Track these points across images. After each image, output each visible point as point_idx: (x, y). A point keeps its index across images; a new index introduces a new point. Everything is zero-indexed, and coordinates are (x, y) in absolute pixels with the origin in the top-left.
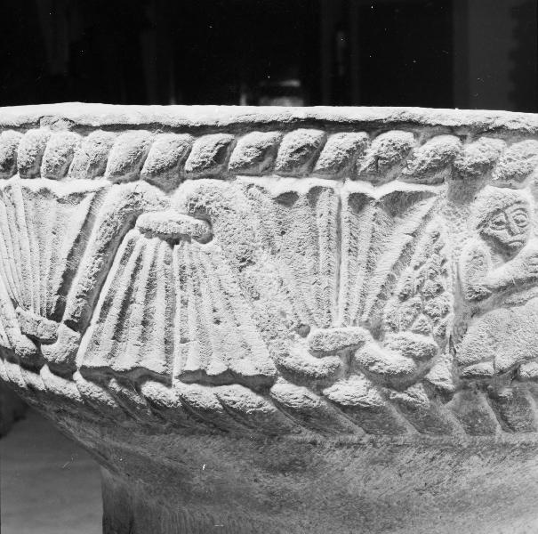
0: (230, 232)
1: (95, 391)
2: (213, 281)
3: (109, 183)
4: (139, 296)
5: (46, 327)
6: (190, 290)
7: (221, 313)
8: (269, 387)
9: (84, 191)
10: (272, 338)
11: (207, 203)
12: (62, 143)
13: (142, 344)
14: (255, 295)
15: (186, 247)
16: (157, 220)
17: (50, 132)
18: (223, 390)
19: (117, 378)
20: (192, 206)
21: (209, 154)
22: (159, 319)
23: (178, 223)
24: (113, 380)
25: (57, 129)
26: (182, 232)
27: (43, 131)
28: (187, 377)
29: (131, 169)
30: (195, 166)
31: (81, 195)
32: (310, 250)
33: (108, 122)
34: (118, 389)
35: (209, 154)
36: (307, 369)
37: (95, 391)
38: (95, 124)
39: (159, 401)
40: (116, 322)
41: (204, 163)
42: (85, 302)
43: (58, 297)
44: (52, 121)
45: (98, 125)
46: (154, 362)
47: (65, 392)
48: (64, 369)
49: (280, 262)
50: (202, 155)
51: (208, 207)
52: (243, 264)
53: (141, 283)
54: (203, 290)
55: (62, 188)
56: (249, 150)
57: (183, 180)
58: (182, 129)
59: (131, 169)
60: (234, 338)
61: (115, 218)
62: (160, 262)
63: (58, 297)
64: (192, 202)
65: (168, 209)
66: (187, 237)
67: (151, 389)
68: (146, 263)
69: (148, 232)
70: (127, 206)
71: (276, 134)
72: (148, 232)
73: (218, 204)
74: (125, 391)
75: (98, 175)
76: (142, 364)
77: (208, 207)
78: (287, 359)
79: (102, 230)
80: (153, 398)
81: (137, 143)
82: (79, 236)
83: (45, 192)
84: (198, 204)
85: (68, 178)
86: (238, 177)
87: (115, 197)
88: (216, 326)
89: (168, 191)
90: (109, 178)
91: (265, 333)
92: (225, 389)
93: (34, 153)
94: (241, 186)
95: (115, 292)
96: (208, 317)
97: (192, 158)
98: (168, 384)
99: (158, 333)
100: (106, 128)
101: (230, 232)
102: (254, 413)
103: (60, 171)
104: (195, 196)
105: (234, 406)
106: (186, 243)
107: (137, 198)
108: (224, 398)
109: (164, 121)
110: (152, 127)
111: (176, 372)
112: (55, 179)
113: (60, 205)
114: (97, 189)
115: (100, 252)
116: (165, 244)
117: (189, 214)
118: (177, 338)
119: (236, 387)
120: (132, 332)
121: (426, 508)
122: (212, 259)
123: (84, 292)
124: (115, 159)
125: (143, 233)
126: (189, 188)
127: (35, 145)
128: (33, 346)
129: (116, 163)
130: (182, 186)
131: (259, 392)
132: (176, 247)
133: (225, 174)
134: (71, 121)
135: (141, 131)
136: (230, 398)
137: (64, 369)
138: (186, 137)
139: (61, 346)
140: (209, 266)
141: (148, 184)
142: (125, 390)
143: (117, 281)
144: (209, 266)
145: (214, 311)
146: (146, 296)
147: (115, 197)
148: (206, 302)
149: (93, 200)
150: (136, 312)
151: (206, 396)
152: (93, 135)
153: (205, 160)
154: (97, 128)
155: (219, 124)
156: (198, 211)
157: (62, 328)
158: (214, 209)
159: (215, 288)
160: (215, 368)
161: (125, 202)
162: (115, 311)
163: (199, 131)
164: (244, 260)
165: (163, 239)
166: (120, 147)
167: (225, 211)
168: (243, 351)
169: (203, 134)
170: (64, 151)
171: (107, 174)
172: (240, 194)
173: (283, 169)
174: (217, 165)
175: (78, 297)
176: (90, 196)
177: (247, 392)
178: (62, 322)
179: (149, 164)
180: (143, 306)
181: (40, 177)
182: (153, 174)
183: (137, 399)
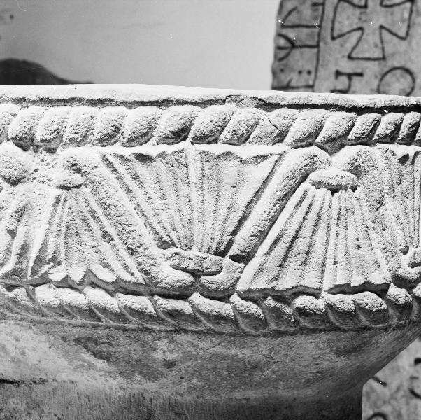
0: (374, 183)
1: (251, 308)
2: (358, 218)
3: (289, 148)
4: (306, 232)
5: (210, 262)
6: (342, 226)
7: (363, 242)
8: (386, 291)
9: (268, 153)
10: (393, 256)
11: (363, 163)
12: (251, 117)
13: (303, 269)
14: (384, 227)
15: (342, 193)
16: (328, 175)
17: (236, 108)
18: (359, 297)
19: (273, 296)
20: (353, 164)
21: (368, 127)
22: (318, 247)
23: (342, 177)
24: (269, 298)
25: (243, 106)
26: (344, 183)
27: (229, 107)
28: (333, 291)
29: (308, 140)
30: (357, 136)
31: (265, 157)
32: (411, 196)
33: (294, 102)
34: (272, 305)
35: (368, 127)
36: (409, 276)
37: (251, 308)
38: (283, 103)
39: (312, 310)
40: (284, 253)
41: (364, 133)
42: (257, 239)
43: (230, 237)
44: (239, 99)
45: (286, 103)
46: (310, 281)
47: (222, 312)
48: (223, 295)
49: (396, 203)
50: (364, 127)
51: (363, 165)
52: (379, 205)
53: (309, 223)
54: (350, 226)
55: (246, 151)
56: (389, 126)
57: (343, 146)
58: (349, 109)
59: (308, 140)
60: (369, 259)
61: (296, 173)
62: (326, 206)
63: (230, 237)
64: (353, 162)
65: (335, 167)
66: (345, 188)
67: (302, 301)
68: (315, 209)
69: (318, 184)
70: (307, 165)
71: (400, 115)
72: (318, 184)
73: (369, 163)
74: (279, 305)
75: (278, 142)
76: (302, 283)
77: (363, 165)
78: (399, 270)
79: (284, 183)
80: (306, 308)
81: (318, 118)
82: (260, 188)
83: (228, 154)
84: (357, 164)
85: (247, 143)
86: (378, 144)
87: (295, 159)
88: (358, 251)
89: (331, 154)
90: (290, 145)
91: (388, 253)
92: (360, 295)
93: (221, 124)
94: (381, 151)
95: (286, 230)
96: (352, 243)
97: (229, 128)
98: (317, 296)
99: (315, 258)
100: (291, 106)
101: (374, 183)
102: (378, 310)
103: (241, 138)
104: (356, 157)
105: (367, 307)
106: (344, 191)
107: (316, 159)
108: (359, 302)
109: (340, 103)
110: (42, 101)
111: (327, 285)
112: (235, 145)
113: (241, 165)
114: (281, 152)
115: (279, 200)
116: (329, 192)
117: (348, 171)
118: (330, 262)
119: (367, 293)
120: (295, 262)
121: (285, 389)
122: (357, 201)
123: (260, 231)
124: (295, 132)
125: (313, 185)
126: (349, 152)
127: (222, 118)
128: (192, 279)
129: (301, 133)
130: (343, 150)
131: (380, 296)
132: (336, 195)
133: (369, 142)
134: (259, 100)
135: (320, 110)
136: (364, 302)
137: (223, 295)
138: (353, 114)
139: (227, 275)
140: (357, 207)
141: (19, 149)
142: (280, 304)
143: (288, 220)
144: (357, 207)
145: (357, 240)
146: (313, 232)
147: (295, 159)
148: (352, 233)
149: (277, 161)
150: (301, 245)
151: (346, 302)
152: (276, 112)
153: (365, 131)
154: (284, 106)
155: (376, 106)
156: (356, 170)
157: (226, 261)
158: (366, 167)
159: (359, 224)
160: (357, 281)
161: (306, 162)
162: (282, 246)
163: (360, 111)
164: (379, 203)
165: (328, 189)
166: (302, 122)
167: (371, 168)
168: (373, 267)
169: (363, 113)
170: (251, 123)
171: (288, 139)
172: (379, 156)
173: (402, 139)
174: (367, 139)
175: (251, 236)
176: (272, 159)
177: (374, 296)
178: (227, 257)
179: (68, 134)
180: (309, 240)
181: (217, 143)
182: (327, 142)
183: (288, 310)
